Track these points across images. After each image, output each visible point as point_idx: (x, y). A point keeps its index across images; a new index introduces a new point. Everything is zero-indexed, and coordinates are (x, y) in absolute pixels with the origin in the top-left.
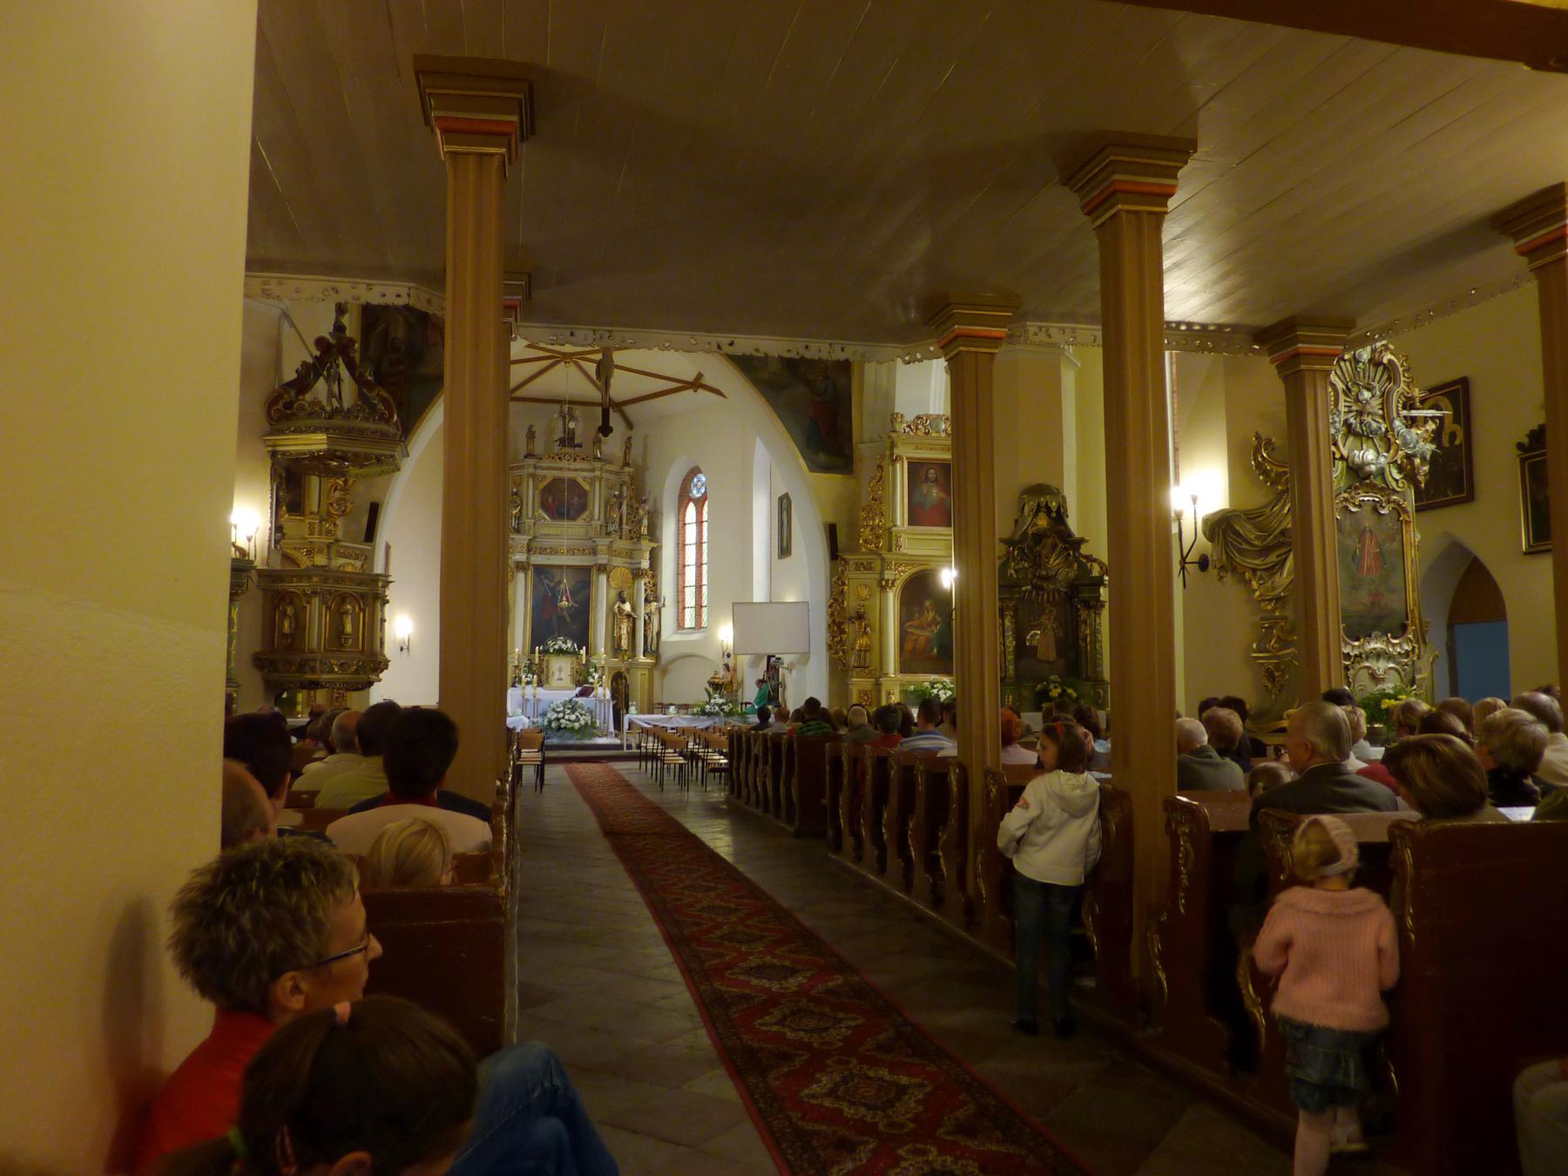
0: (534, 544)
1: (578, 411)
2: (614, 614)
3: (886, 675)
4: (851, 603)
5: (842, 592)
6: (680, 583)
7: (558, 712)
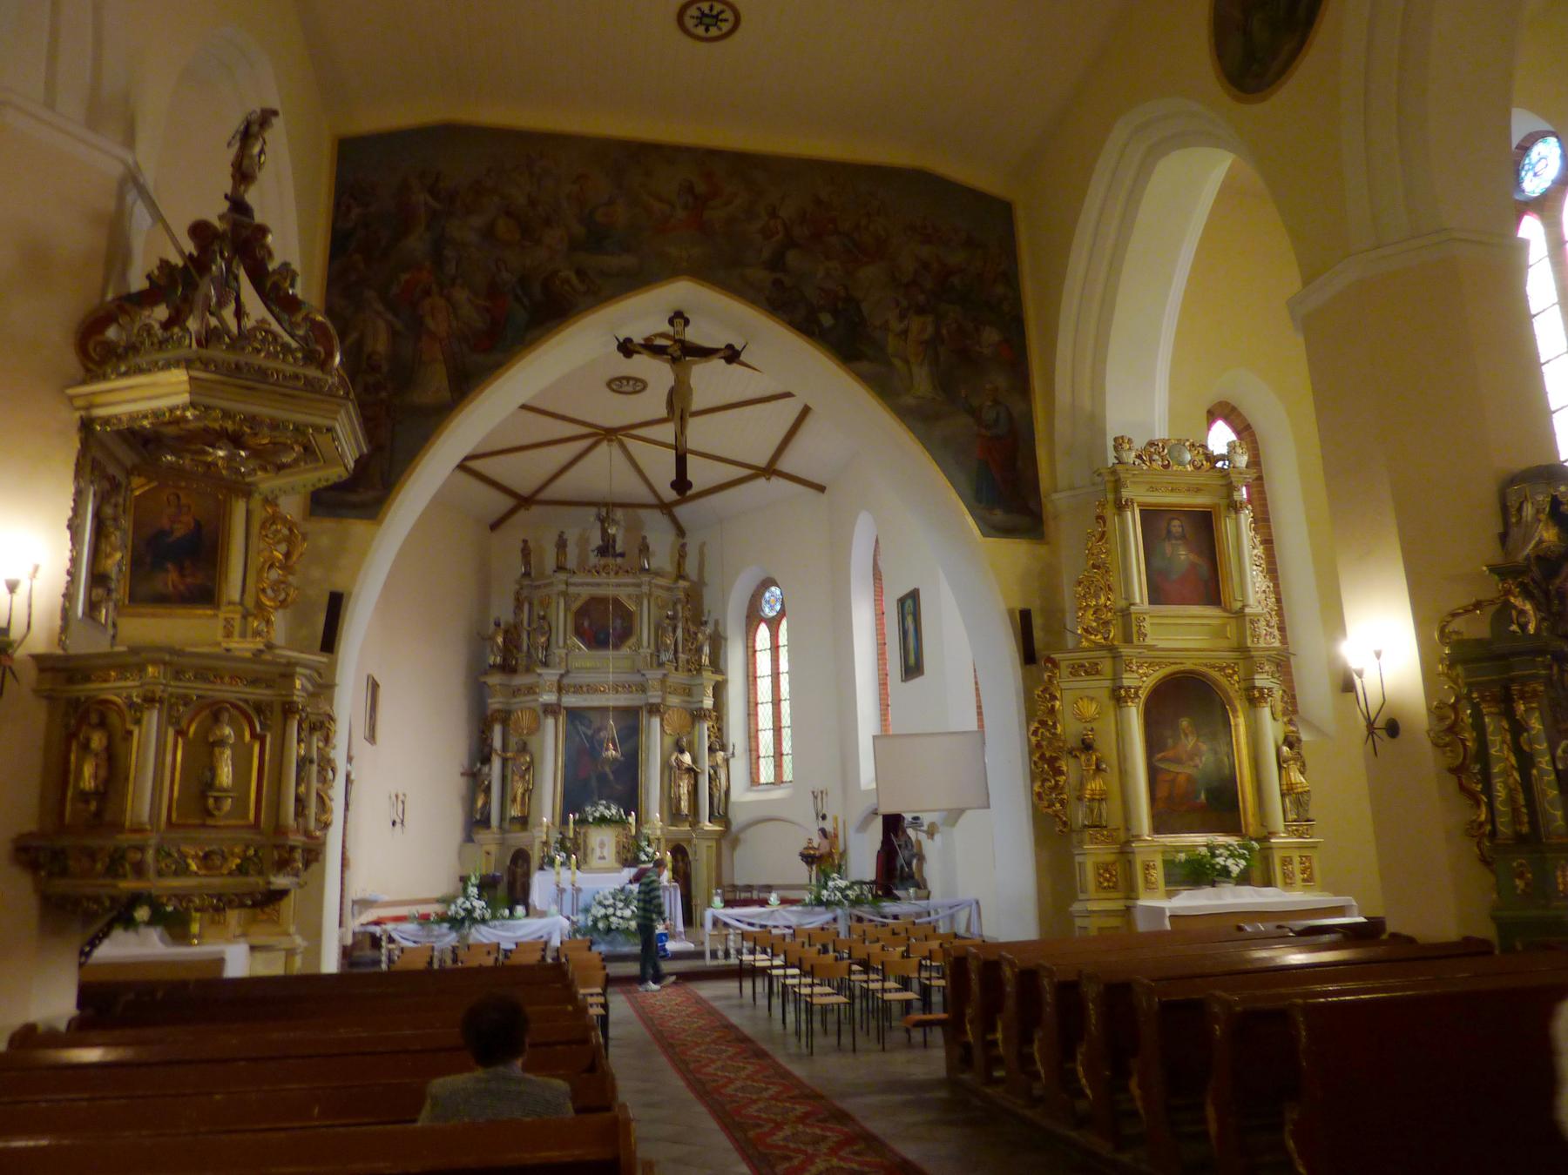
0: (565, 681)
1: (619, 514)
2: (671, 768)
3: (1138, 838)
4: (1069, 728)
5: (1052, 710)
6: (752, 726)
7: (606, 907)
